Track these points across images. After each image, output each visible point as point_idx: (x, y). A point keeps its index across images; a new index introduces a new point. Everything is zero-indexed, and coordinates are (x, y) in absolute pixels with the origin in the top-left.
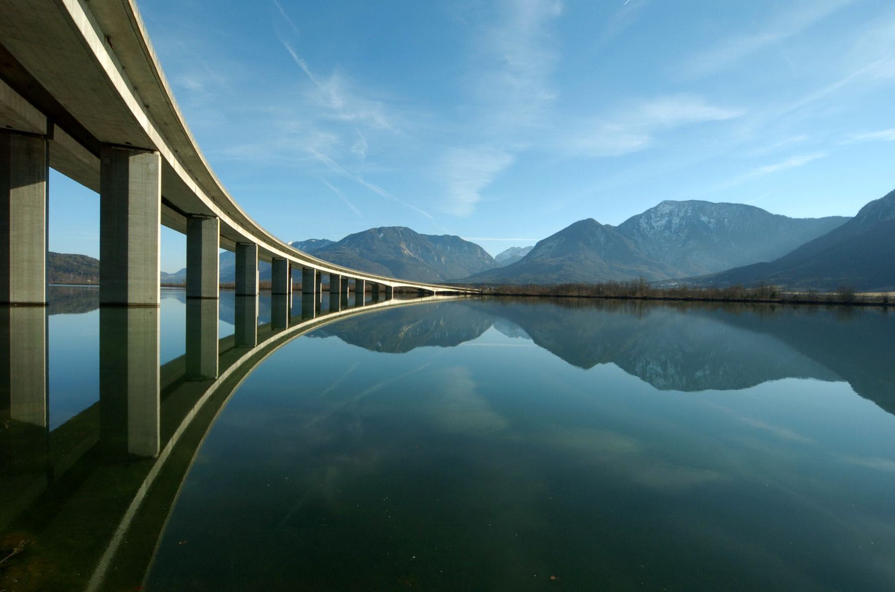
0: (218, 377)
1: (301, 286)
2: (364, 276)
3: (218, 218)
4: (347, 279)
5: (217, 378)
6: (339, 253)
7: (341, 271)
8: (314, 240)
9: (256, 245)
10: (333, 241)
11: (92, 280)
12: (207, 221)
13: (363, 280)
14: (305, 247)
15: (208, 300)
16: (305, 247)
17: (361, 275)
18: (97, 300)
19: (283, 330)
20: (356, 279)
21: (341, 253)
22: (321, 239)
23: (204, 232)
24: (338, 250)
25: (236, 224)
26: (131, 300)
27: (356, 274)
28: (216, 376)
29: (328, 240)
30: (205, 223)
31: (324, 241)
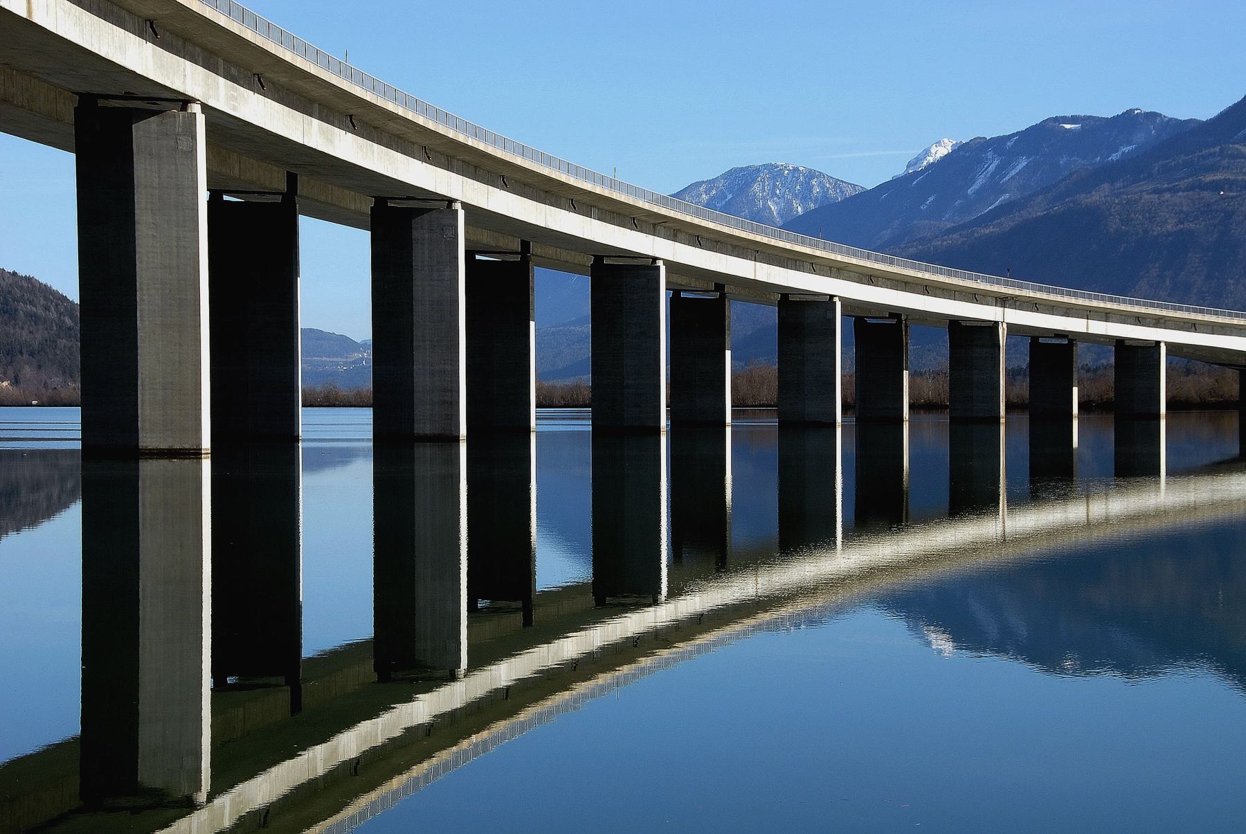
0: (211, 797)
1: (770, 392)
2: (1159, 322)
3: (196, 108)
4: (1071, 342)
5: (202, 797)
6: (1216, 186)
7: (1003, 301)
8: (1073, 120)
9: (458, 206)
10: (1183, 116)
11: (16, 381)
12: (153, 122)
13: (1158, 343)
14: (1023, 163)
15: (163, 463)
16: (1023, 163)
17: (1139, 320)
18: (74, 481)
19: (637, 606)
20: (1120, 344)
21: (1229, 184)
22: (1108, 110)
23: (144, 172)
24: (1213, 168)
25: (316, 122)
26: (147, 440)
27: (1106, 316)
28: (198, 788)
29: (1152, 116)
30: (143, 132)
31: (1129, 121)
